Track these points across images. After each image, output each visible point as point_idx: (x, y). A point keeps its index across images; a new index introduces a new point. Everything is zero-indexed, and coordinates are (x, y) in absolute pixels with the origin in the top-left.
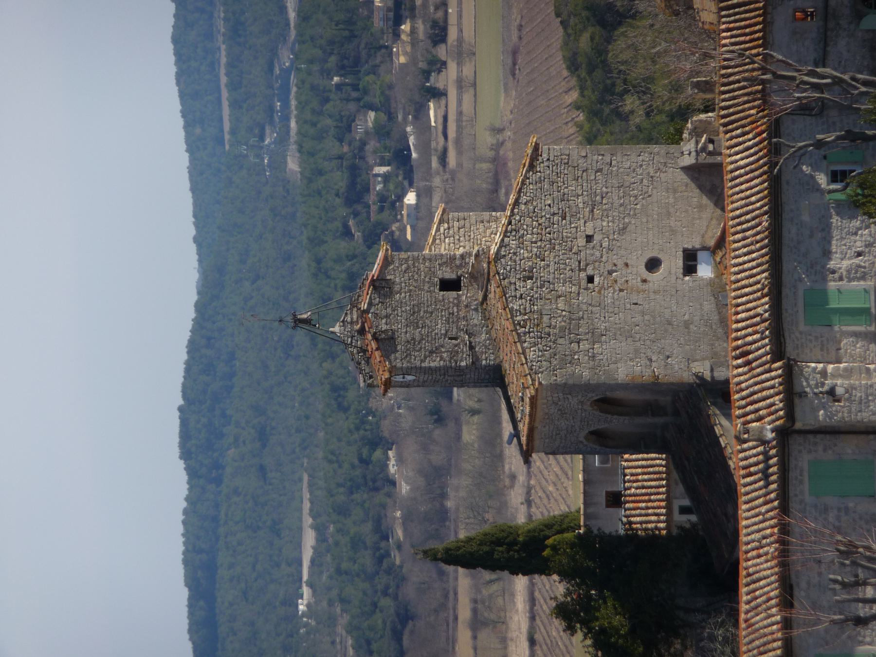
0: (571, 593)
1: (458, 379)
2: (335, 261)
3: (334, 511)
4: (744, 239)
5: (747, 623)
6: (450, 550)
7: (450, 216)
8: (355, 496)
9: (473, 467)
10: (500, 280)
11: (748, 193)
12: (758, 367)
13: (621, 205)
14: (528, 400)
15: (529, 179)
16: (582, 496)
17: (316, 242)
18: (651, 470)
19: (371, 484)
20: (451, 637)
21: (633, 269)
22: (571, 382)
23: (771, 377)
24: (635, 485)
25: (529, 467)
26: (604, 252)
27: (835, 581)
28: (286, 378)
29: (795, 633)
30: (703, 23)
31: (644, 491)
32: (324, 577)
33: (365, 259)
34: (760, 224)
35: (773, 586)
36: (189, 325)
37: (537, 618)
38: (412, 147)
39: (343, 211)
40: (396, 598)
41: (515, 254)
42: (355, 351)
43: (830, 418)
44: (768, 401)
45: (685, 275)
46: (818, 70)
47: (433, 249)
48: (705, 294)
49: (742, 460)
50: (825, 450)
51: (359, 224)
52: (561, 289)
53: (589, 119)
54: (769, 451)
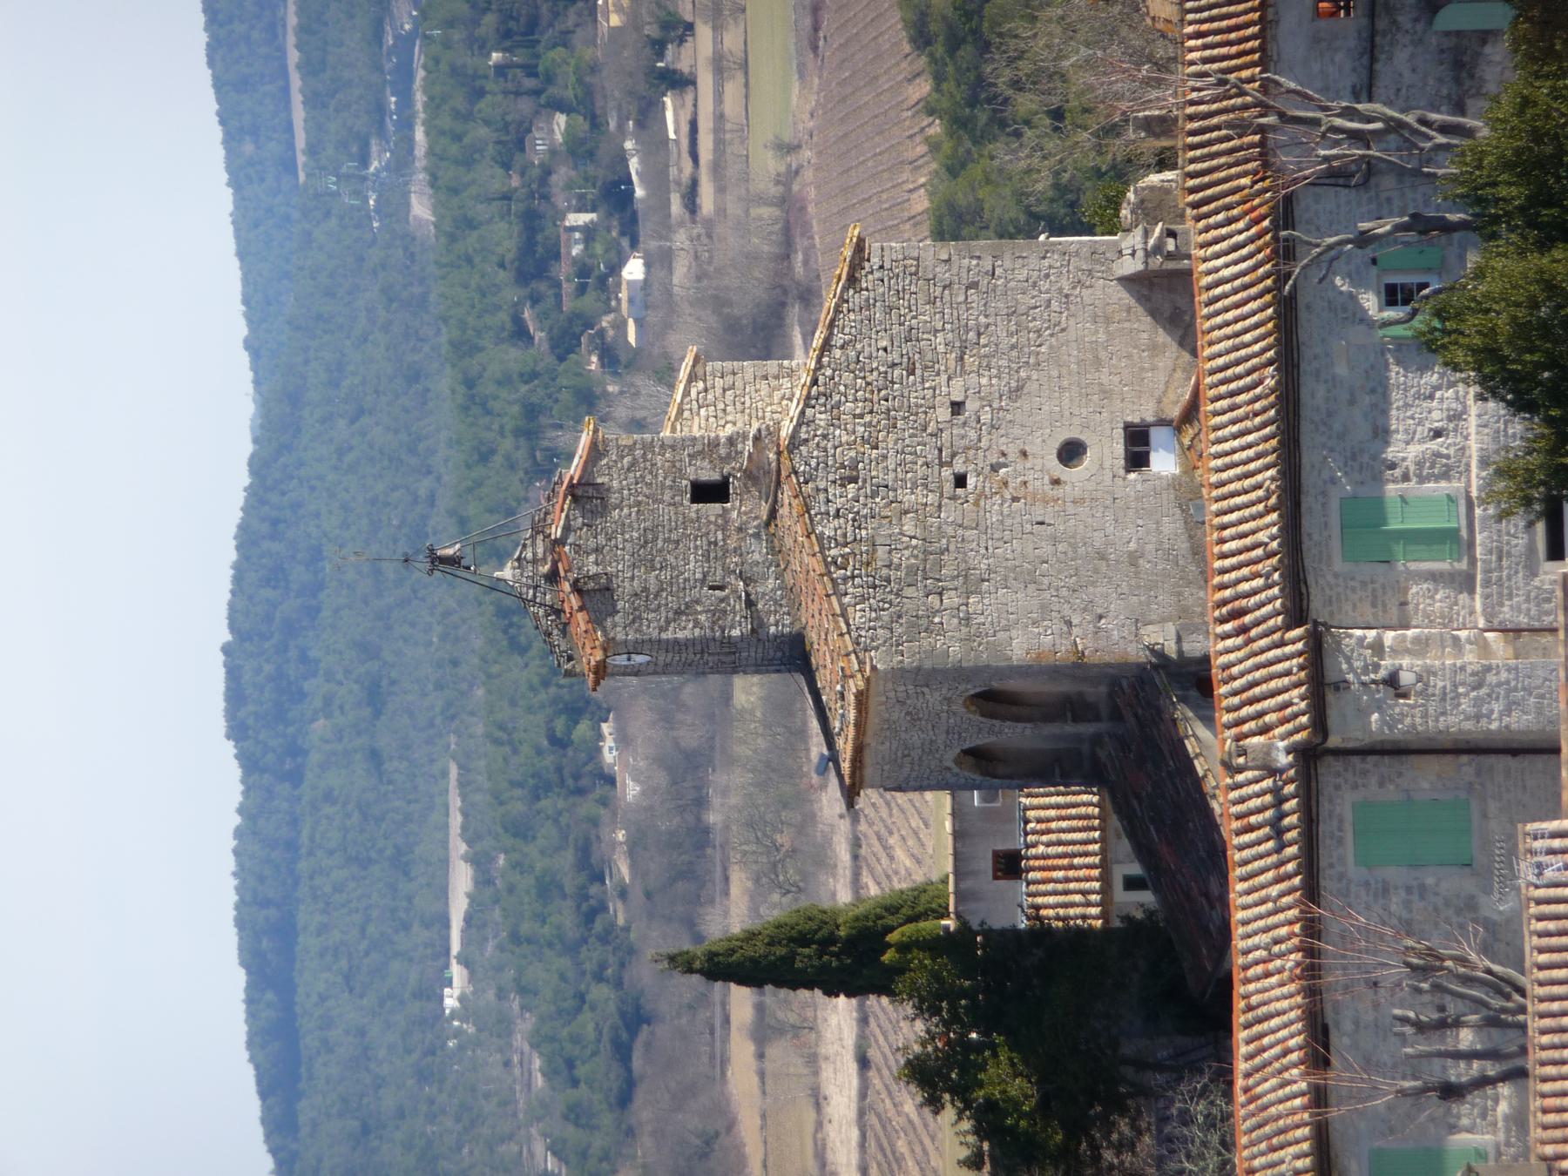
0: (933, 1039)
1: (729, 659)
2: (499, 383)
3: (506, 829)
4: (1232, 408)
5: (1249, 1094)
6: (717, 954)
7: (709, 369)
8: (544, 803)
9: (755, 751)
10: (799, 483)
11: (1239, 326)
12: (1261, 637)
13: (1013, 347)
14: (852, 697)
15: (847, 302)
16: (951, 859)
17: (464, 349)
18: (1073, 811)
19: (570, 782)
20: (718, 1056)
21: (1036, 461)
22: (928, 665)
23: (1284, 654)
24: (1044, 838)
25: (855, 820)
26: (984, 432)
27: (1404, 1020)
28: (414, 591)
29: (1334, 1113)
30: (1153, 18)
31: (1060, 849)
32: (490, 947)
33: (553, 380)
34: (1261, 382)
35: (1294, 1028)
36: (239, 498)
37: (872, 1020)
38: (635, 178)
39: (512, 294)
40: (619, 984)
41: (825, 437)
42: (541, 612)
43: (1391, 728)
44: (1280, 699)
45: (1128, 471)
46: (1359, 107)
47: (678, 427)
48: (1165, 503)
49: (1235, 803)
50: (1381, 784)
51: (542, 317)
52: (908, 499)
53: (951, 134)
54: (1282, 788)
